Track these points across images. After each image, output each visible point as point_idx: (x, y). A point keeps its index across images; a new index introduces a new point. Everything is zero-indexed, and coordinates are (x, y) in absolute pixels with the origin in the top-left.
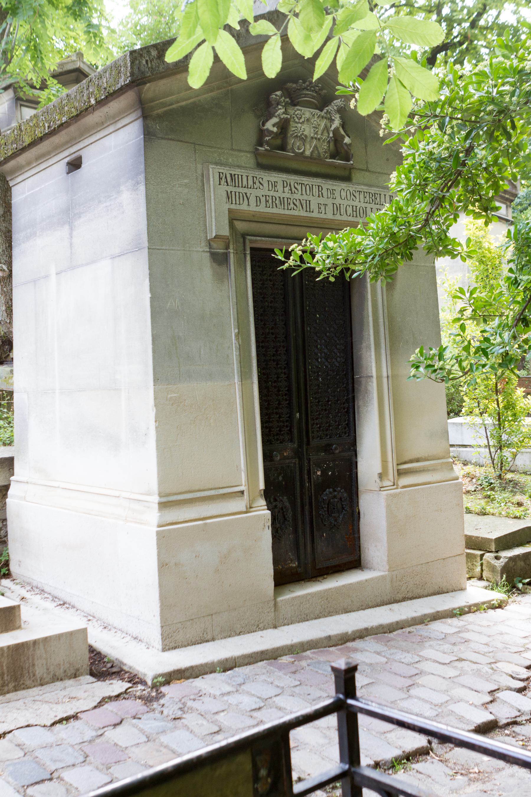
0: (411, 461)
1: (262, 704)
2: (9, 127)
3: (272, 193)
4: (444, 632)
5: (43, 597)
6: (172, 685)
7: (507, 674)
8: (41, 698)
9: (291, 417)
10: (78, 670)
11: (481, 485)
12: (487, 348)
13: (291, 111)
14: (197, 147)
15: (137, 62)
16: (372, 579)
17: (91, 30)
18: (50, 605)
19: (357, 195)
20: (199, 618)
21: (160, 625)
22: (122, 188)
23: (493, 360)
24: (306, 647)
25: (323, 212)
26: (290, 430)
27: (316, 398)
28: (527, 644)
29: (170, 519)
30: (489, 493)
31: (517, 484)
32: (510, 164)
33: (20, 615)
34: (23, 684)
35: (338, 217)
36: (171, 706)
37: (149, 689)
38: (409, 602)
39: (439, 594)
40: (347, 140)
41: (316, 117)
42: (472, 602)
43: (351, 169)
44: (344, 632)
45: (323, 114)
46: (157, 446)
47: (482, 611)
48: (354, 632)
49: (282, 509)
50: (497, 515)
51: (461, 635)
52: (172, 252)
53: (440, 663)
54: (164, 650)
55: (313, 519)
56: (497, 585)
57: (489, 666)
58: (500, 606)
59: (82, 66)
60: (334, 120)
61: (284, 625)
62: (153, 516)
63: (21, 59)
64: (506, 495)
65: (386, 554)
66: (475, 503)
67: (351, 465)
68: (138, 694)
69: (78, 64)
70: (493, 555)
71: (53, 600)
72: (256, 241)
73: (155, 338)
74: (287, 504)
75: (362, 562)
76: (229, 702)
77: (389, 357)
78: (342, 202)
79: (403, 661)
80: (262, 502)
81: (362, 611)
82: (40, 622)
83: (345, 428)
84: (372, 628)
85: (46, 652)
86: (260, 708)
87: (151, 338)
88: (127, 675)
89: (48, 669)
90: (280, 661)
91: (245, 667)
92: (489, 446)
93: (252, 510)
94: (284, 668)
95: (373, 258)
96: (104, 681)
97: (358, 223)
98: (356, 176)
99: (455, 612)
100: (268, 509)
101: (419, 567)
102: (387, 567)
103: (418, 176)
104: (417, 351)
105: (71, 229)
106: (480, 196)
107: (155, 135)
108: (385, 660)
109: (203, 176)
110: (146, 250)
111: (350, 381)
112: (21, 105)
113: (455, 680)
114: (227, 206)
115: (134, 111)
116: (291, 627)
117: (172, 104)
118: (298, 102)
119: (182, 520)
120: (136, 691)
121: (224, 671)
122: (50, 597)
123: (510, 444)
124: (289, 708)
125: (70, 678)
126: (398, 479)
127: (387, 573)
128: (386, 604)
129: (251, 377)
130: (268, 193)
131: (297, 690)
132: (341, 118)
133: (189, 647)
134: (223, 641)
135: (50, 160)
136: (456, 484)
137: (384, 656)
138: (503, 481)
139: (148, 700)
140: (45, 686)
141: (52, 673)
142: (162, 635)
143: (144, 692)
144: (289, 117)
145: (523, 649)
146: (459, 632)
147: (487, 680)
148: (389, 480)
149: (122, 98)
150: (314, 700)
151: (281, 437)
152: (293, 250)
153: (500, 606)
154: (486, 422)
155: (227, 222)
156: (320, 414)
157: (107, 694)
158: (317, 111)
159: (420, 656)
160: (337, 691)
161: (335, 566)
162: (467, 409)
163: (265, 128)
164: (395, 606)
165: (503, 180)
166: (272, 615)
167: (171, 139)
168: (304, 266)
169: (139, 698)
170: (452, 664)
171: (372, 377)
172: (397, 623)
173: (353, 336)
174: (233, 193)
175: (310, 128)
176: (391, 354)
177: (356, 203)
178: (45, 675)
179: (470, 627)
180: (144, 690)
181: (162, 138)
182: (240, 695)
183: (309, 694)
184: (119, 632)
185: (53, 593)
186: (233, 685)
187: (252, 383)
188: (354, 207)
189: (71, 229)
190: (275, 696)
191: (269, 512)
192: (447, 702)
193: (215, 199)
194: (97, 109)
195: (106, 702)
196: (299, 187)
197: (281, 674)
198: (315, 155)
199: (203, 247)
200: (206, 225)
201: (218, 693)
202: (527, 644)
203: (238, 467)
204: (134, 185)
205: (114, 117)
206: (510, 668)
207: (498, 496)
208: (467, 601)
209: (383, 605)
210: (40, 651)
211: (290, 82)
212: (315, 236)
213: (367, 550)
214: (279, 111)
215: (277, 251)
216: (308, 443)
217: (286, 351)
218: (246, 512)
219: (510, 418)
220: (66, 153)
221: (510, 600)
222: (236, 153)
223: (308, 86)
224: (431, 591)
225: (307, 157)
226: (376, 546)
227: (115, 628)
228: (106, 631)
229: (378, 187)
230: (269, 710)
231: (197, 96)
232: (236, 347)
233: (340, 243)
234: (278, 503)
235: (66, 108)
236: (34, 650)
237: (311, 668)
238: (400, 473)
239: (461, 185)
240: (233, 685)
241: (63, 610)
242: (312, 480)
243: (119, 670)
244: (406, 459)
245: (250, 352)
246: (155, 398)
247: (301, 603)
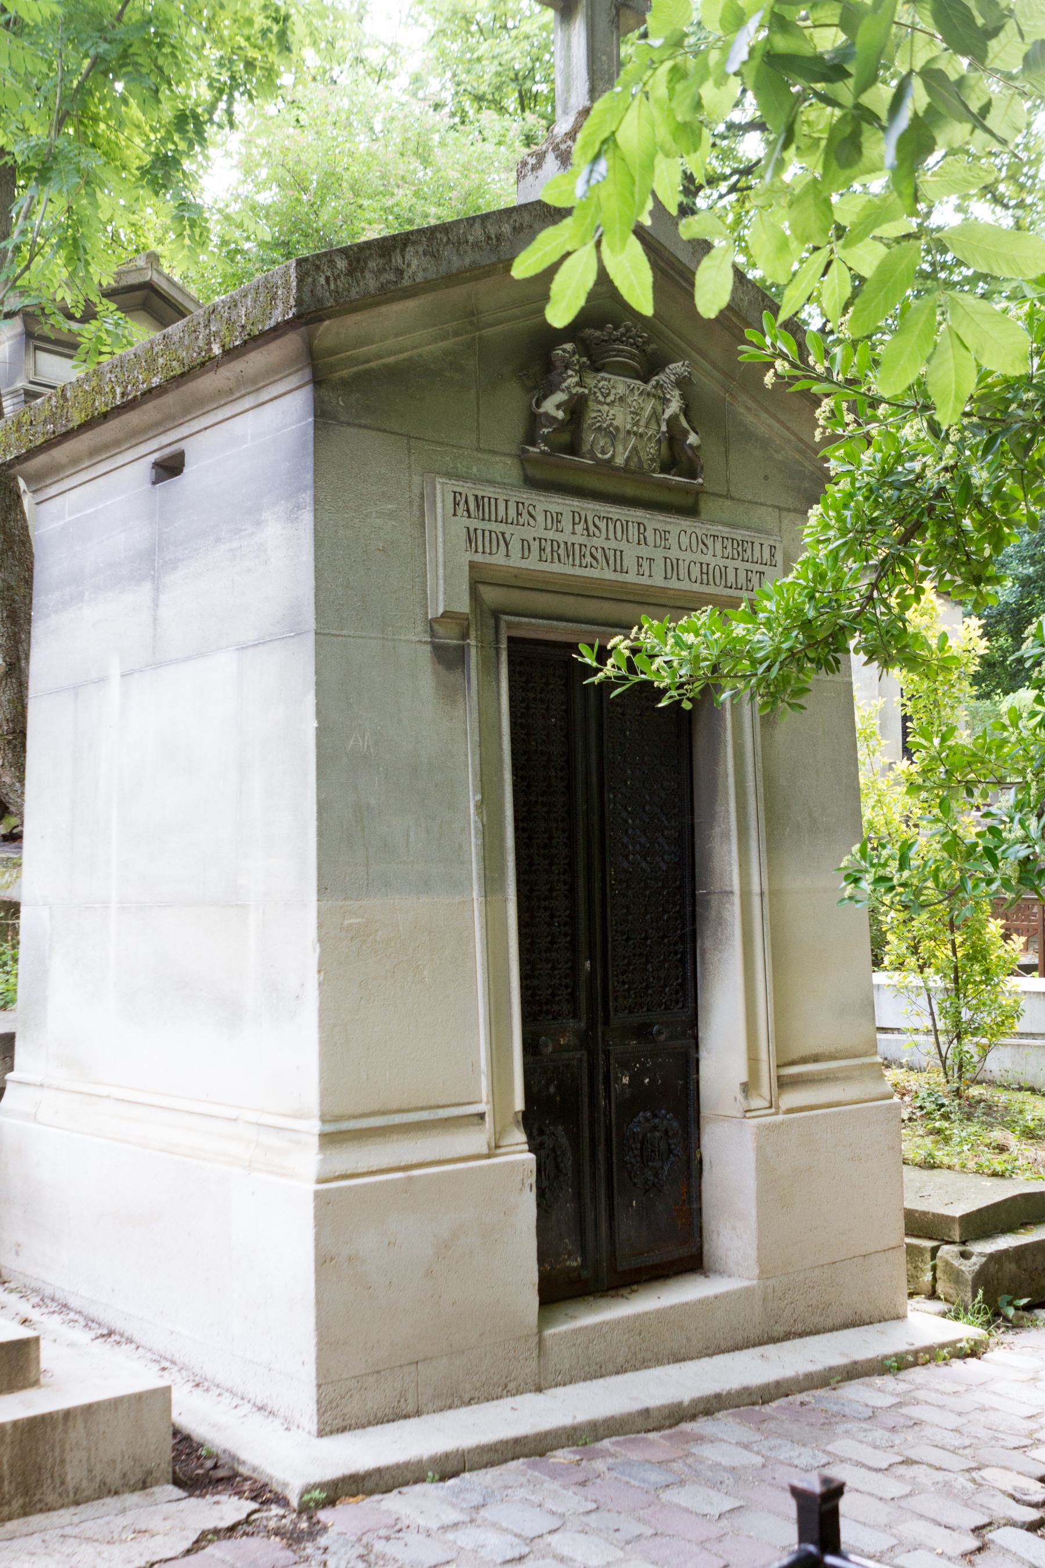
0: (804, 1060)
1: (525, 1550)
2: (10, 389)
3: (551, 535)
4: (870, 1403)
5: (67, 1318)
6: (339, 1507)
7: (1004, 1492)
8: (76, 1531)
9: (574, 969)
10: (149, 1473)
11: (921, 1108)
12: (996, 848)
13: (591, 380)
14: (413, 442)
15: (310, 280)
16: (727, 1295)
17: (186, 215)
18: (82, 1336)
19: (709, 542)
20: (392, 1369)
21: (314, 1382)
22: (266, 515)
23: (1009, 868)
24: (601, 1431)
25: (647, 573)
26: (572, 994)
27: (623, 933)
28: (1036, 1431)
30: (937, 1124)
31: (990, 1107)
32: (1025, 496)
33: (38, 1358)
34: (40, 1501)
35: (673, 584)
36: (343, 1550)
37: (294, 1515)
38: (798, 1342)
39: (854, 1326)
40: (693, 439)
41: (637, 393)
42: (920, 1343)
43: (698, 493)
44: (676, 1400)
45: (649, 388)
46: (321, 1021)
47: (941, 1363)
48: (695, 1402)
49: (554, 1150)
50: (957, 1168)
51: (905, 1410)
52: (360, 641)
53: (870, 1468)
54: (321, 1433)
55: (614, 1172)
56: (966, 1310)
57: (967, 1475)
58: (974, 1352)
59: (156, 278)
60: (669, 400)
61: (556, 1386)
62: (307, 1162)
63: (48, 263)
64: (973, 1128)
66: (915, 1144)
67: (687, 1064)
68: (272, 1524)
69: (149, 275)
70: (956, 1249)
71: (86, 1325)
72: (519, 625)
73: (323, 808)
74: (564, 1141)
75: (705, 1259)
76: (459, 1543)
77: (764, 854)
78: (682, 555)
79: (796, 1462)
80: (520, 1137)
81: (707, 1359)
82: (76, 1375)
83: (677, 992)
84: (729, 1394)
85: (88, 1434)
86: (521, 1558)
87: (314, 808)
88: (247, 1485)
89: (90, 1471)
90: (552, 1460)
91: (483, 1471)
92: (936, 1031)
94: (561, 1475)
95: (769, 668)
96: (203, 1496)
97: (741, 600)
98: (709, 506)
99: (888, 1363)
100: (530, 1151)
101: (817, 1271)
102: (756, 1271)
103: (858, 516)
104: (856, 848)
105: (157, 590)
106: (967, 555)
107: (335, 418)
108: (758, 1460)
109: (422, 498)
111: (688, 900)
112: (36, 348)
113: (904, 1503)
114: (466, 557)
115: (296, 371)
116: (570, 1388)
118: (604, 365)
119: (365, 1170)
120: (268, 1519)
121: (443, 1478)
122: (81, 1319)
123: (977, 1029)
124: (579, 1559)
125: (133, 1490)
126: (779, 1095)
127: (755, 1282)
128: (754, 1346)
129: (503, 889)
130: (544, 534)
131: (593, 1520)
132: (683, 396)
133: (370, 1429)
134: (438, 1417)
135: (119, 457)
136: (890, 1108)
137: (758, 1453)
138: (965, 1101)
139: (294, 1538)
140: (82, 1507)
141: (98, 1479)
142: (318, 1402)
143: (284, 1521)
144: (586, 391)
145: (1028, 1442)
146: (900, 1405)
147: (967, 1505)
149: (273, 346)
150: (628, 1543)
151: (556, 1007)
152: (614, 648)
153: (974, 1353)
154: (931, 984)
155: (466, 586)
156: (629, 964)
157: (210, 1525)
158: (639, 382)
159: (829, 1453)
160: (803, 1538)
161: (654, 1267)
162: (893, 958)
163: (542, 410)
164: (770, 1349)
165: (1009, 527)
166: (534, 1364)
167: (366, 427)
168: (635, 679)
169: (276, 1535)
170: (893, 1469)
171: (732, 892)
172: (778, 1384)
173: (696, 811)
174: (480, 533)
175: (625, 413)
176: (769, 850)
177: (707, 558)
178: (85, 1483)
179: (921, 1395)
180: (284, 1517)
181: (349, 424)
182: (478, 1531)
183: (617, 1530)
184: (226, 1394)
185: (85, 1312)
186: (462, 1510)
187: (506, 900)
188: (705, 566)
189: (157, 590)
190: (550, 1532)
191: (532, 1156)
192: (892, 1548)
194: (223, 364)
195: (210, 1541)
196: (602, 525)
197: (555, 1486)
198: (633, 465)
199: (418, 634)
200: (425, 592)
201: (434, 1525)
202: (1036, 1431)
203: (475, 1066)
204: (292, 511)
205: (254, 381)
206: (1010, 1481)
207: (956, 1130)
208: (911, 1341)
209: (748, 1347)
210: (77, 1433)
211: (589, 327)
212: (656, 622)
213: (715, 1236)
214: (569, 381)
215: (583, 648)
216: (606, 1021)
217: (568, 838)
218: (488, 1156)
219: (978, 979)
220: (153, 444)
221: (992, 1341)
222: (486, 456)
223: (623, 335)
224: (839, 1320)
226: (734, 1228)
227: (218, 1386)
228: (199, 1391)
229: (748, 528)
230: (541, 1562)
231: (416, 348)
232: (476, 828)
233: (705, 636)
234: (545, 1138)
235: (161, 361)
236: (65, 1431)
237: (614, 1474)
238: (784, 1084)
239: (928, 535)
240: (462, 1510)
241: (108, 1346)
242: (613, 1095)
243: (231, 1473)
244: (795, 1055)
245: (502, 839)
246: (320, 926)
247: (591, 1341)
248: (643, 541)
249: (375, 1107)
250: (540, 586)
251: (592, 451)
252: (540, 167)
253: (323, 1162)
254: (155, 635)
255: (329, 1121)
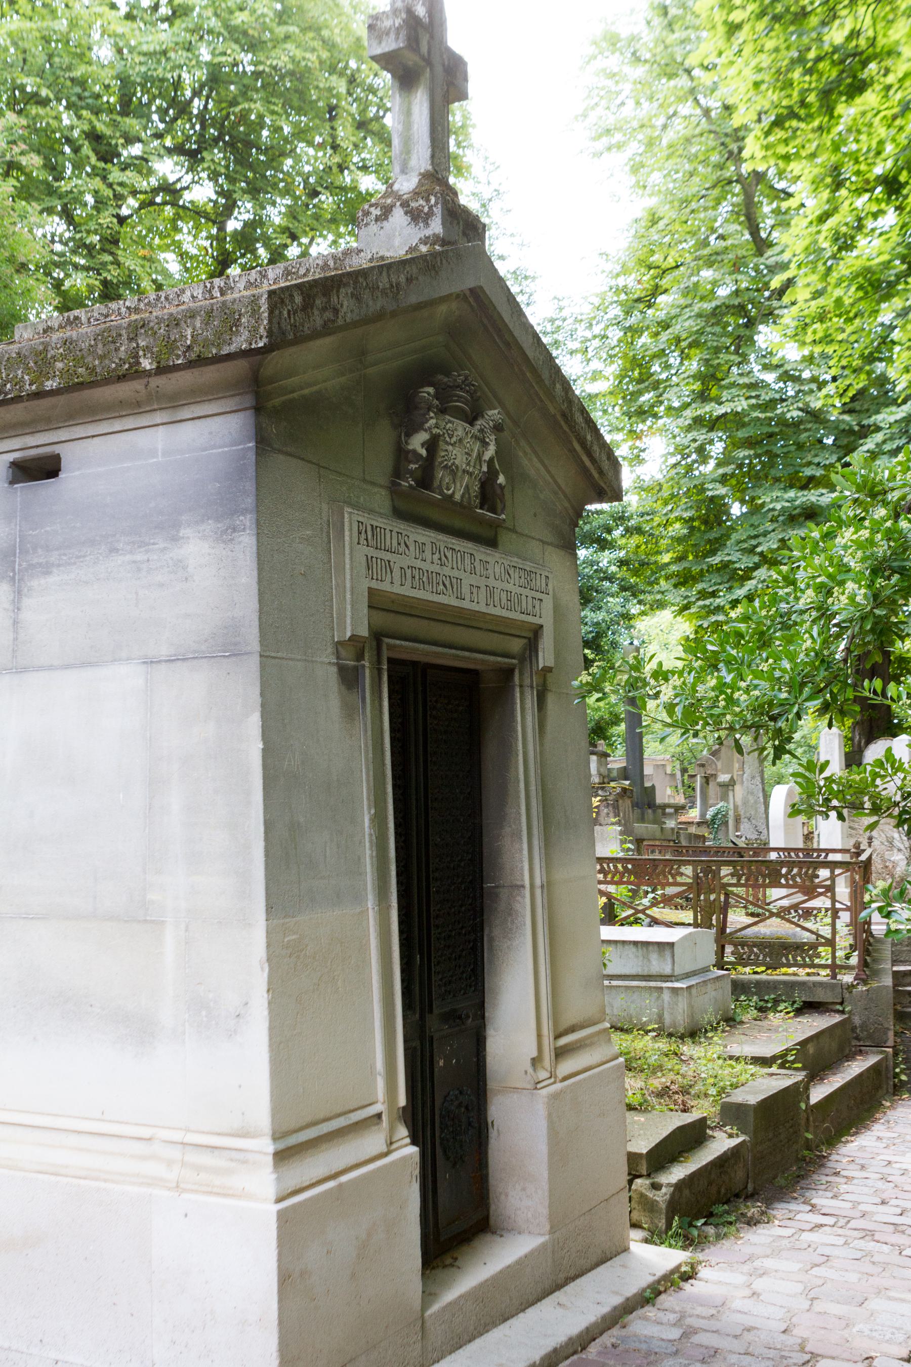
14: (322, 471)
29: (292, 1184)
40: (501, 479)
43: (496, 526)
52: (291, 663)
60: (488, 444)
65: (547, 1203)
84: (561, 1346)
87: (262, 829)
93: (394, 1146)
98: (505, 538)
102: (548, 1227)
110: (256, 659)
117: (293, 392)
119: (308, 1183)
148: (543, 1068)
171: (523, 886)
177: (510, 587)
189: (19, 593)
191: (414, 1150)
193: (352, 569)
196: (449, 554)
199: (327, 656)
203: (373, 1067)
204: (225, 532)
213: (503, 1197)
218: (386, 1154)
220: (16, 443)
224: (594, 1259)
225: (455, 504)
226: (524, 1189)
238: (560, 1053)
246: (268, 946)
248: (473, 572)
249: (308, 1119)
250: (407, 611)
251: (440, 486)
252: (386, 218)
253: (278, 1179)
254: (15, 639)
255: (279, 1138)
